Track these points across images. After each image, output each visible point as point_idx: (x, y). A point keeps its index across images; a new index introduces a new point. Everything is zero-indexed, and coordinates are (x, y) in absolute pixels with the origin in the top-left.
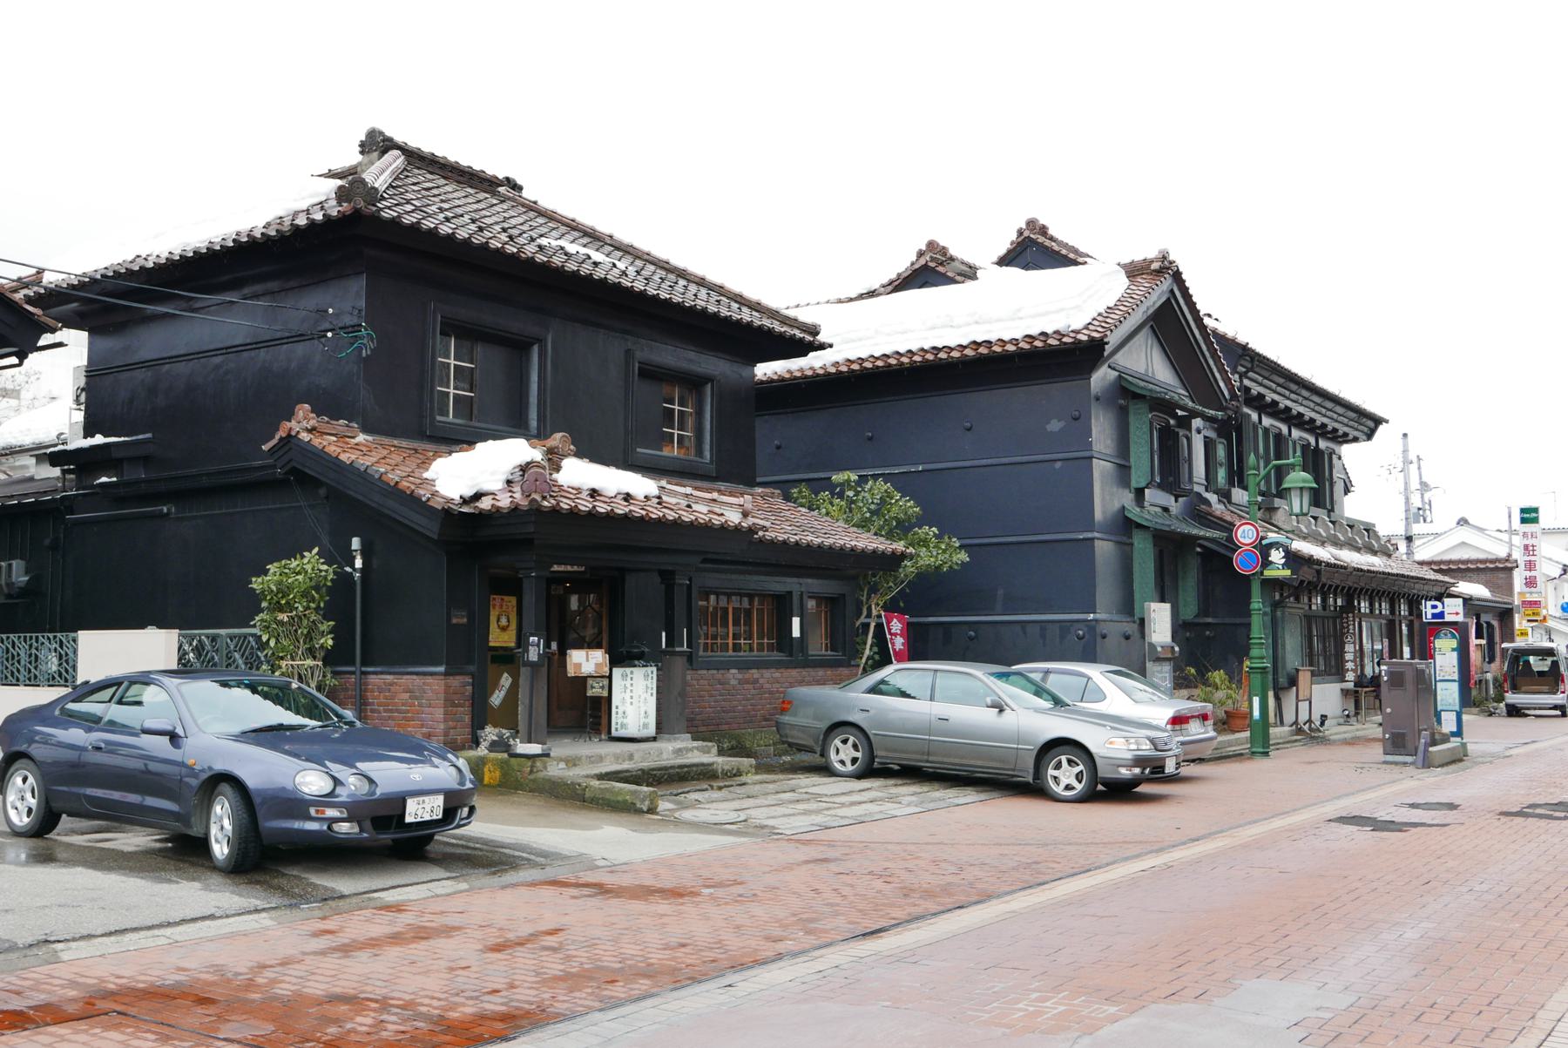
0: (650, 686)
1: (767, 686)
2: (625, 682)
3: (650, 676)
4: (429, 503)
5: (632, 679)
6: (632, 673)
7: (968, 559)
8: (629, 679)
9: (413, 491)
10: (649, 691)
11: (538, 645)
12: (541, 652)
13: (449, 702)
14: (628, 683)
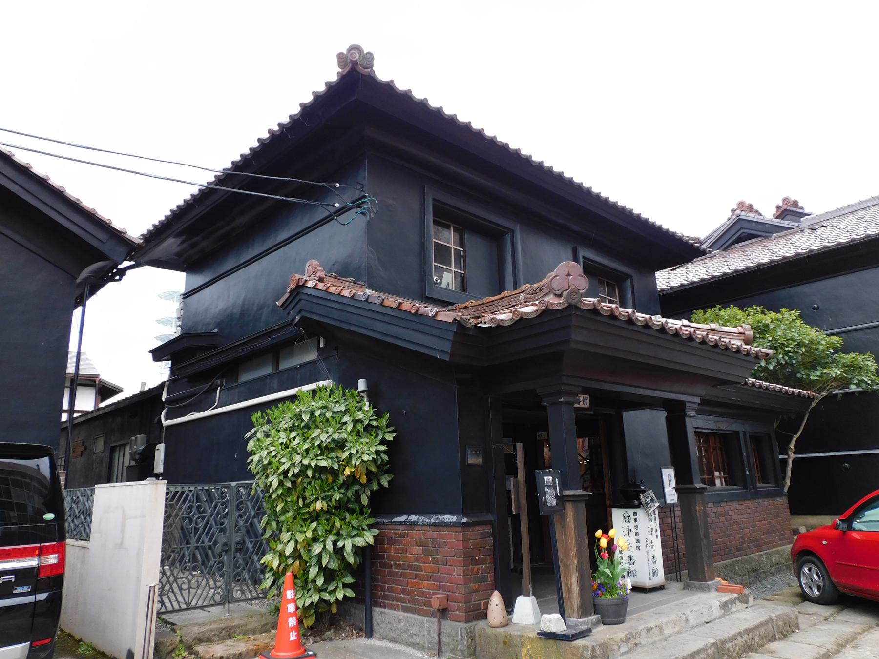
0: (653, 527)
1: (734, 517)
2: (628, 524)
3: (653, 516)
4: (437, 318)
5: (636, 521)
6: (635, 514)
7: (388, 487)
8: (632, 521)
9: (418, 308)
10: (654, 533)
11: (554, 486)
12: (559, 495)
13: (469, 559)
14: (632, 525)
